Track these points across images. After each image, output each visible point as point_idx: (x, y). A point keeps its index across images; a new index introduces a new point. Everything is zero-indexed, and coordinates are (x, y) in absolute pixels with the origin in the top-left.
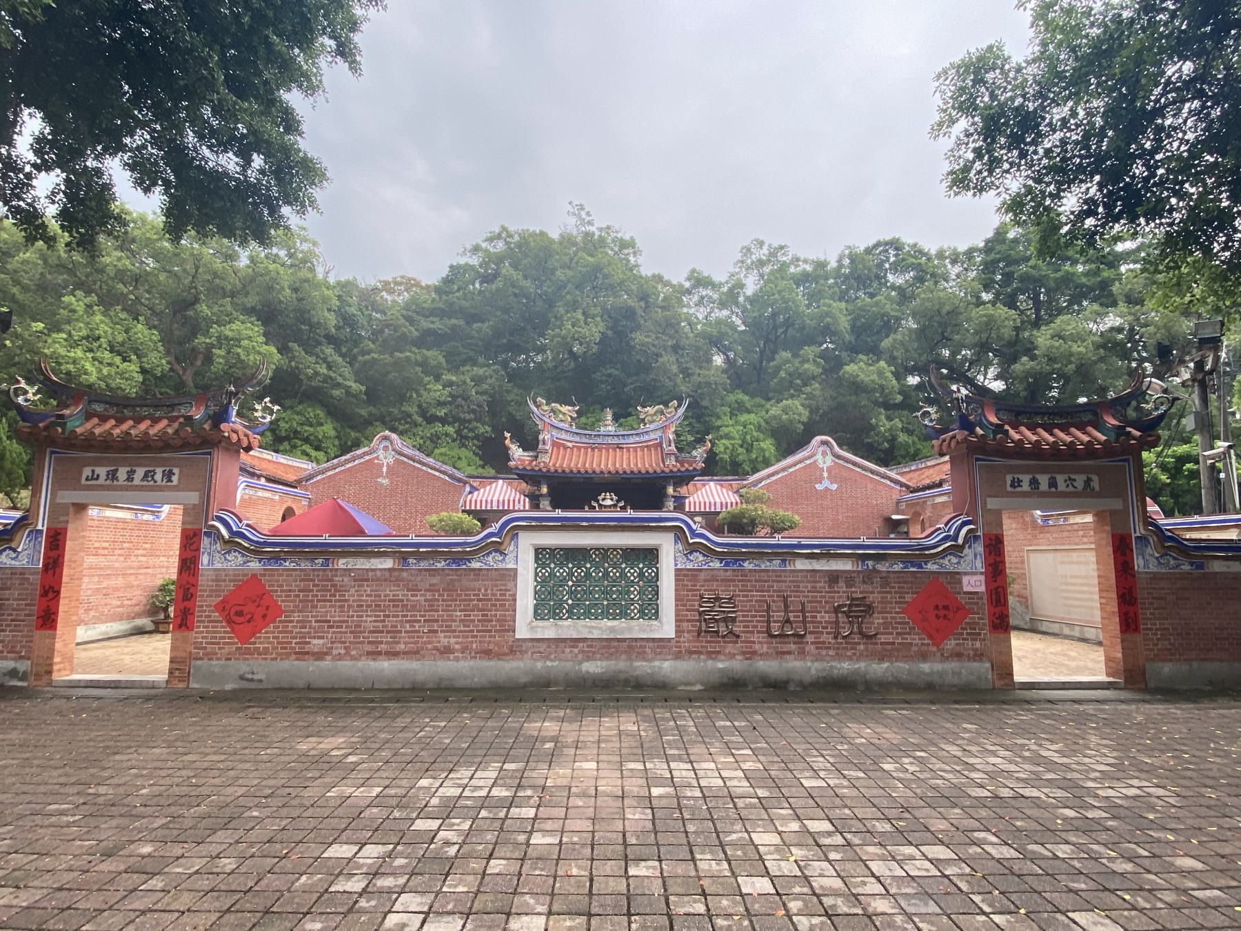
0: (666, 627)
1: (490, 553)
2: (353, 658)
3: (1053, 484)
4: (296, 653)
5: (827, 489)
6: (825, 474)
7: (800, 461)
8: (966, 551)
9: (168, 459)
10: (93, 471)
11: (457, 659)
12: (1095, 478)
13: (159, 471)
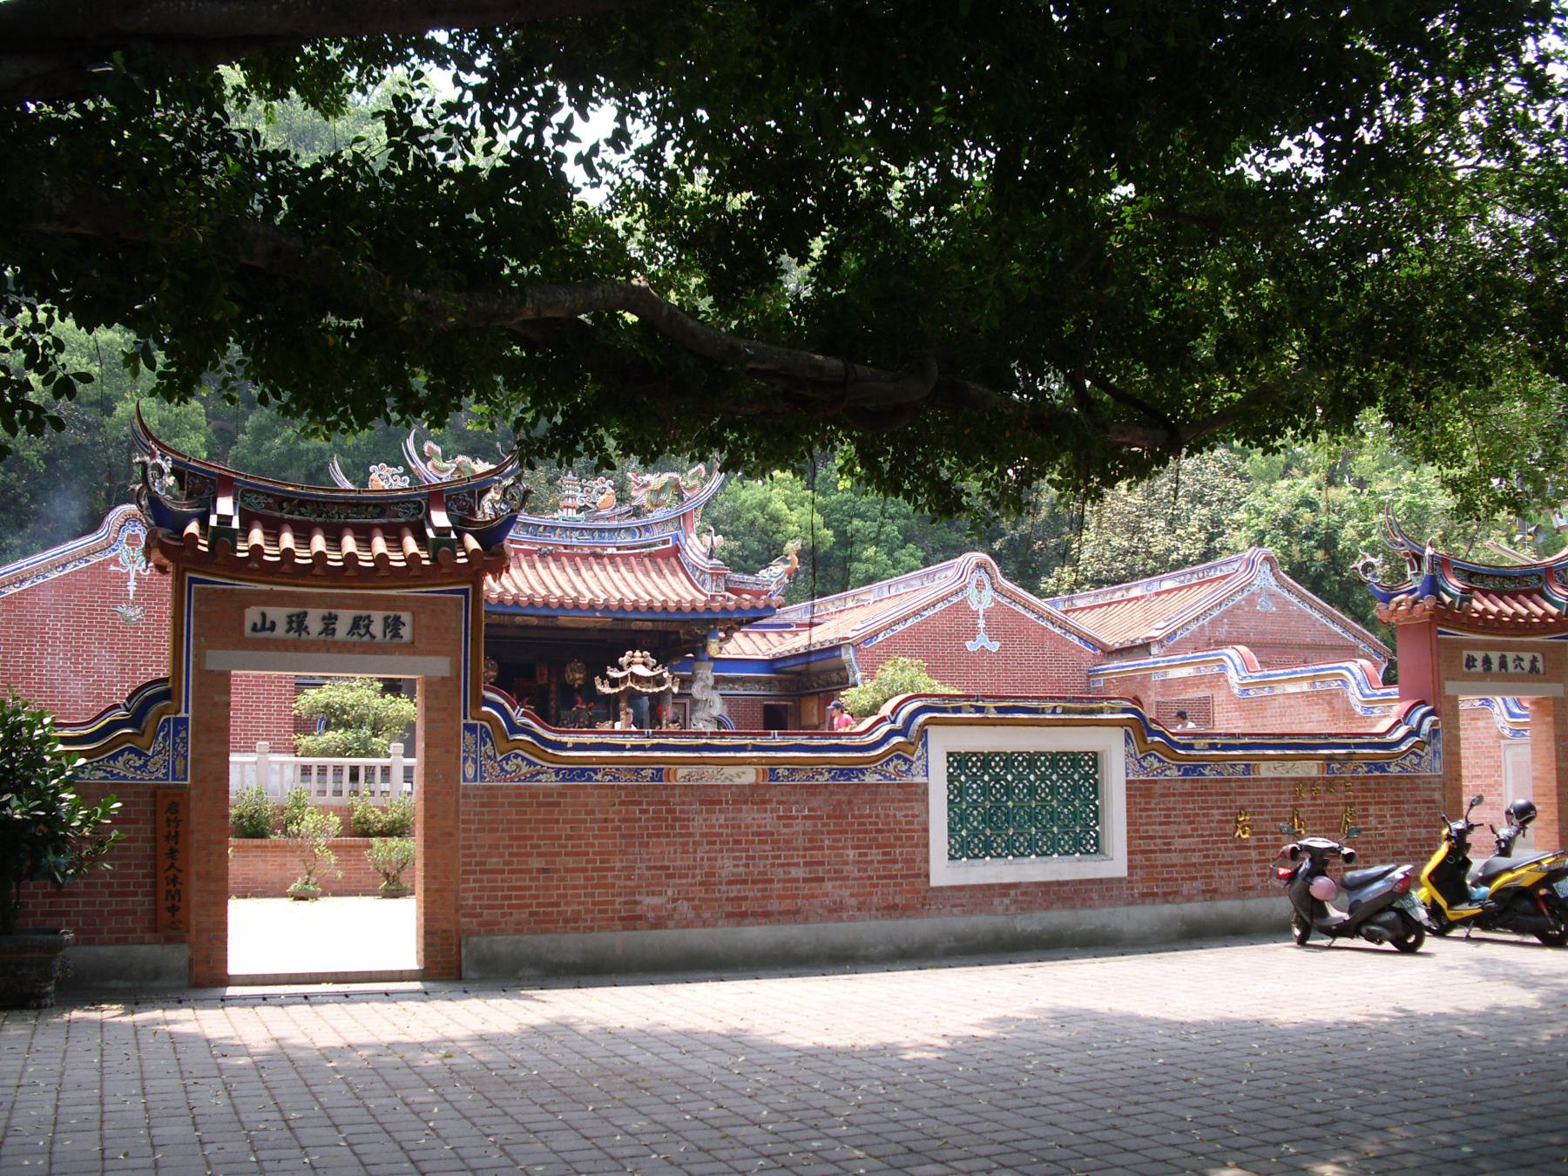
0: (1114, 864)
1: (121, 753)
2: (705, 924)
4: (622, 919)
5: (983, 651)
6: (981, 623)
9: (395, 598)
10: (264, 615)
11: (852, 918)
12: (1540, 657)
13: (378, 617)
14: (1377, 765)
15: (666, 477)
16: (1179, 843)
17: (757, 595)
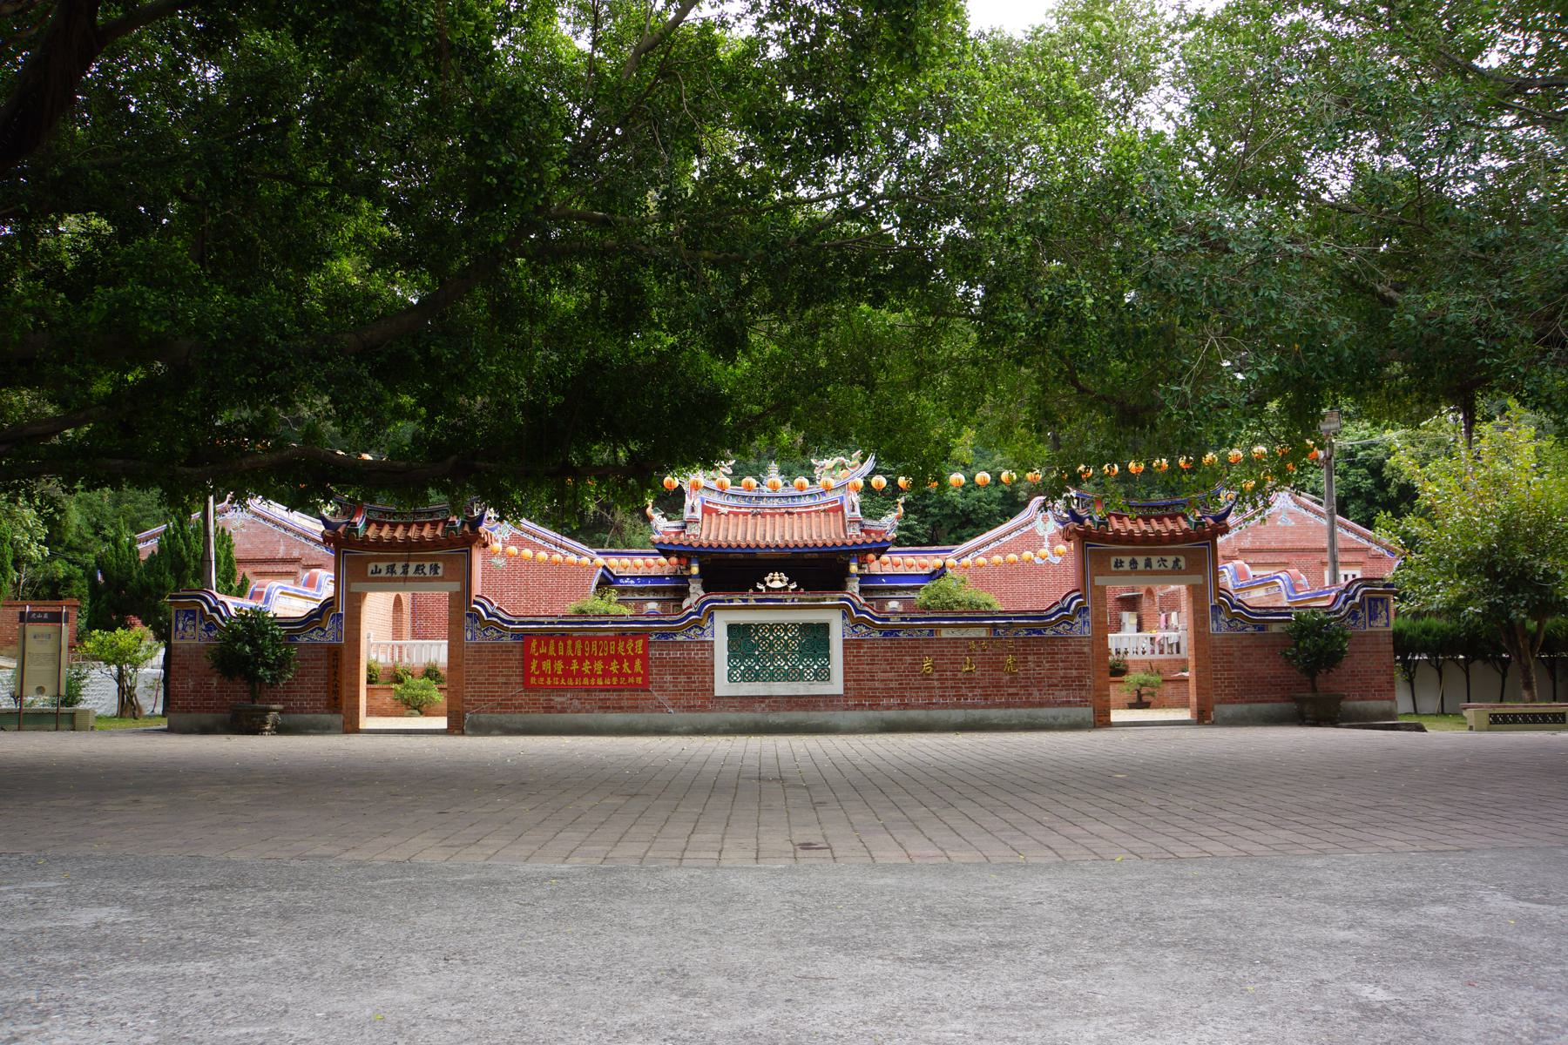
0: (836, 686)
3: (1148, 563)
7: (1016, 529)
8: (1077, 619)
12: (1182, 558)
13: (427, 565)
14: (1031, 629)
15: (836, 460)
16: (880, 676)
17: (879, 533)
